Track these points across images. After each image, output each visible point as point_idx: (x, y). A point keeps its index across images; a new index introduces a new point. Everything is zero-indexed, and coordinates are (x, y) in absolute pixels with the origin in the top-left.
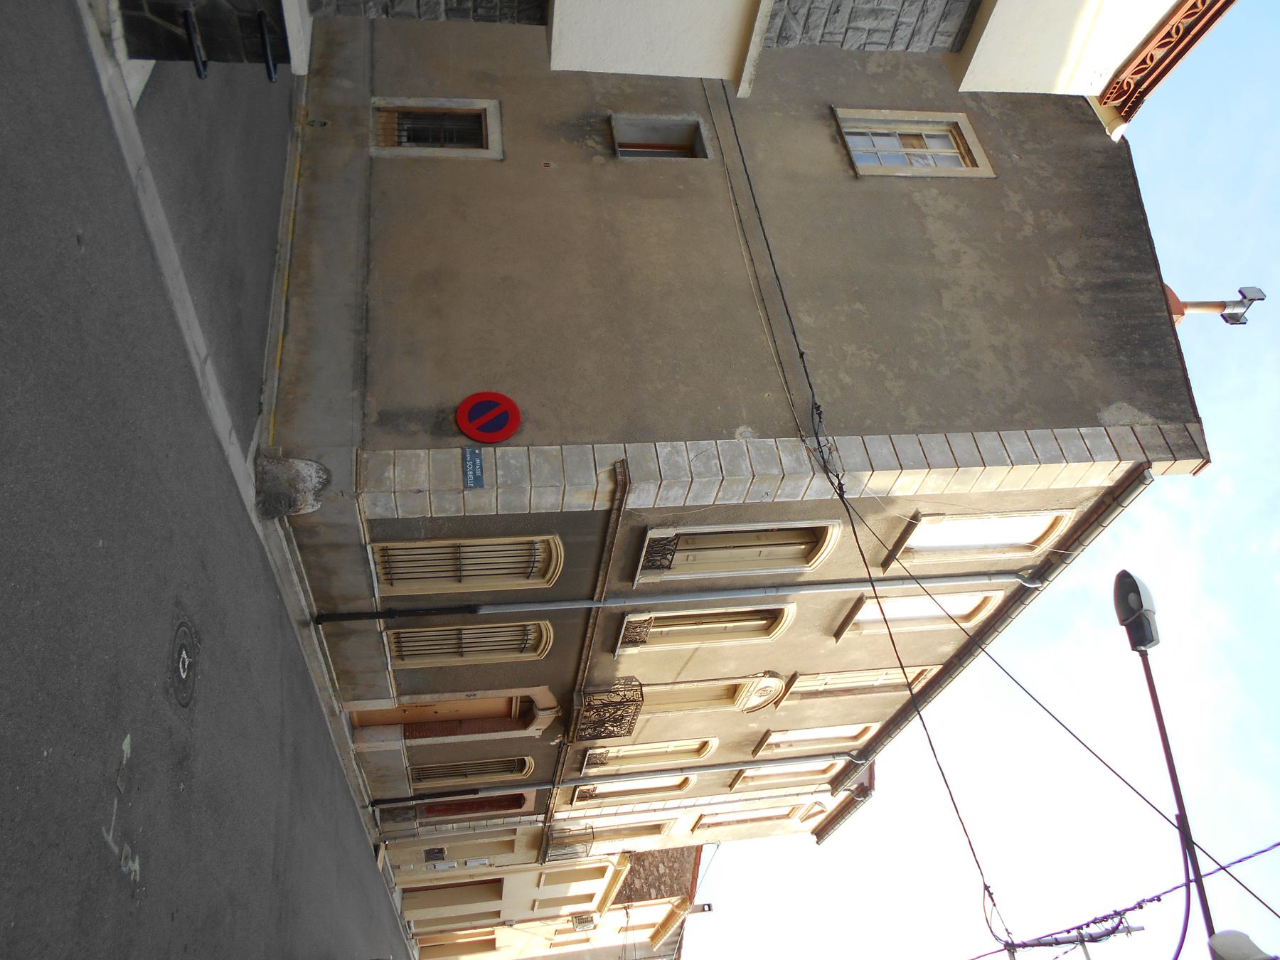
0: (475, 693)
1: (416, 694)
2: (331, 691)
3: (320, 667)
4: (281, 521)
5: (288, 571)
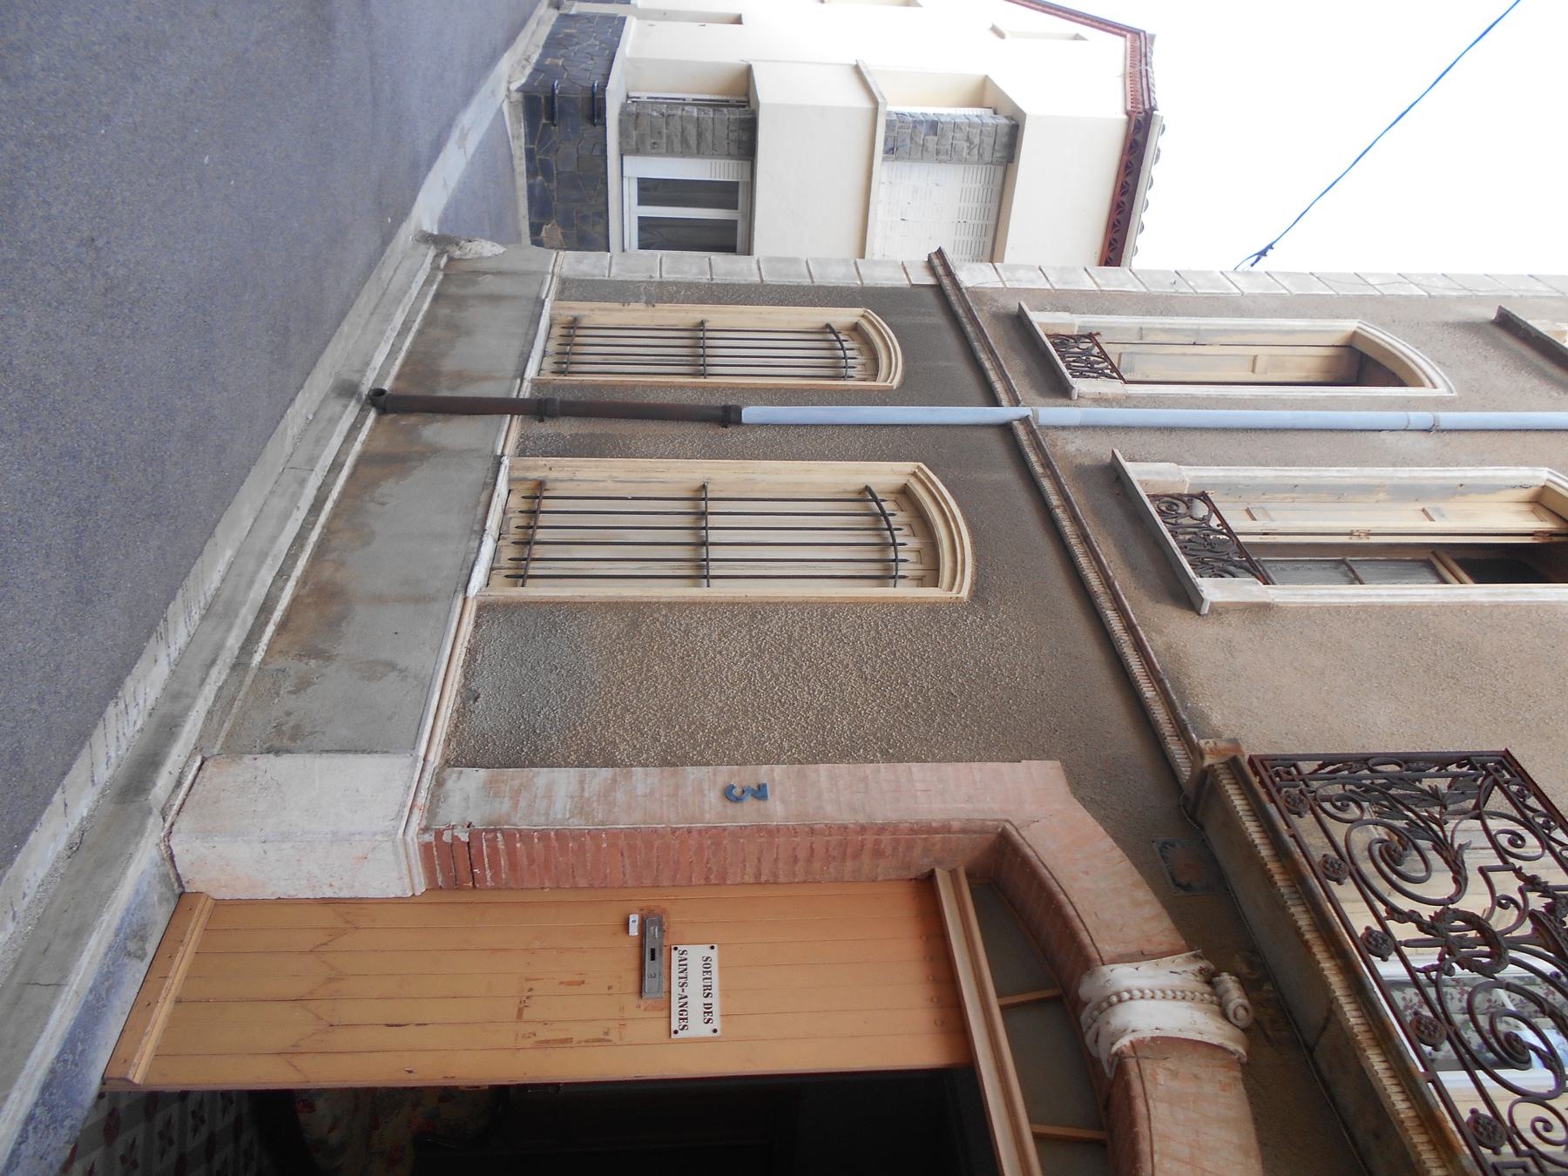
0: (764, 773)
1: (516, 764)
2: (234, 641)
3: (286, 516)
4: (438, 256)
5: (398, 301)
